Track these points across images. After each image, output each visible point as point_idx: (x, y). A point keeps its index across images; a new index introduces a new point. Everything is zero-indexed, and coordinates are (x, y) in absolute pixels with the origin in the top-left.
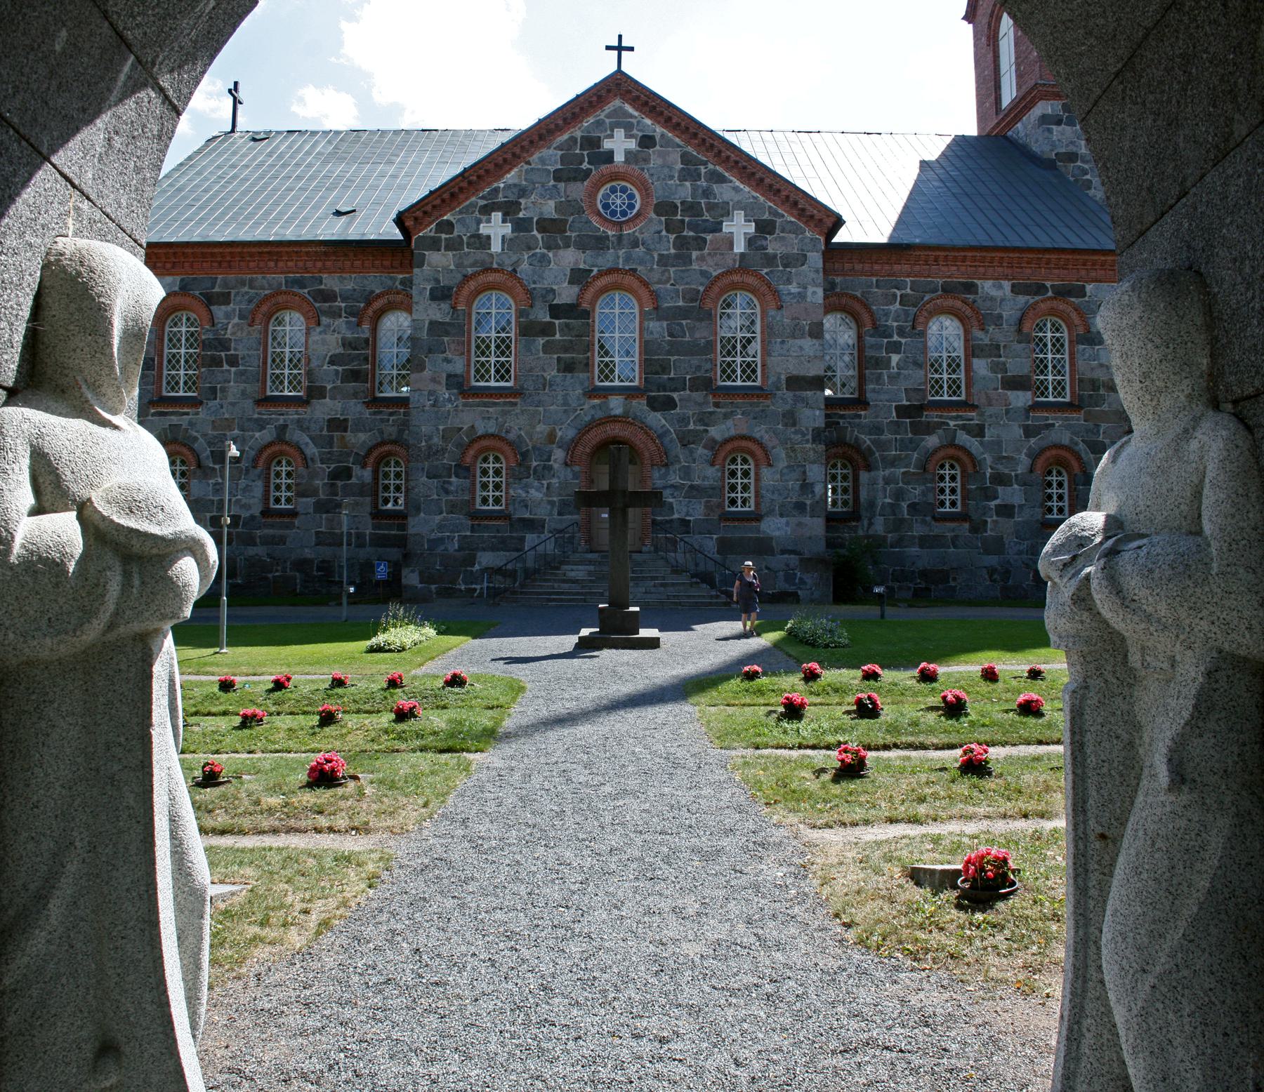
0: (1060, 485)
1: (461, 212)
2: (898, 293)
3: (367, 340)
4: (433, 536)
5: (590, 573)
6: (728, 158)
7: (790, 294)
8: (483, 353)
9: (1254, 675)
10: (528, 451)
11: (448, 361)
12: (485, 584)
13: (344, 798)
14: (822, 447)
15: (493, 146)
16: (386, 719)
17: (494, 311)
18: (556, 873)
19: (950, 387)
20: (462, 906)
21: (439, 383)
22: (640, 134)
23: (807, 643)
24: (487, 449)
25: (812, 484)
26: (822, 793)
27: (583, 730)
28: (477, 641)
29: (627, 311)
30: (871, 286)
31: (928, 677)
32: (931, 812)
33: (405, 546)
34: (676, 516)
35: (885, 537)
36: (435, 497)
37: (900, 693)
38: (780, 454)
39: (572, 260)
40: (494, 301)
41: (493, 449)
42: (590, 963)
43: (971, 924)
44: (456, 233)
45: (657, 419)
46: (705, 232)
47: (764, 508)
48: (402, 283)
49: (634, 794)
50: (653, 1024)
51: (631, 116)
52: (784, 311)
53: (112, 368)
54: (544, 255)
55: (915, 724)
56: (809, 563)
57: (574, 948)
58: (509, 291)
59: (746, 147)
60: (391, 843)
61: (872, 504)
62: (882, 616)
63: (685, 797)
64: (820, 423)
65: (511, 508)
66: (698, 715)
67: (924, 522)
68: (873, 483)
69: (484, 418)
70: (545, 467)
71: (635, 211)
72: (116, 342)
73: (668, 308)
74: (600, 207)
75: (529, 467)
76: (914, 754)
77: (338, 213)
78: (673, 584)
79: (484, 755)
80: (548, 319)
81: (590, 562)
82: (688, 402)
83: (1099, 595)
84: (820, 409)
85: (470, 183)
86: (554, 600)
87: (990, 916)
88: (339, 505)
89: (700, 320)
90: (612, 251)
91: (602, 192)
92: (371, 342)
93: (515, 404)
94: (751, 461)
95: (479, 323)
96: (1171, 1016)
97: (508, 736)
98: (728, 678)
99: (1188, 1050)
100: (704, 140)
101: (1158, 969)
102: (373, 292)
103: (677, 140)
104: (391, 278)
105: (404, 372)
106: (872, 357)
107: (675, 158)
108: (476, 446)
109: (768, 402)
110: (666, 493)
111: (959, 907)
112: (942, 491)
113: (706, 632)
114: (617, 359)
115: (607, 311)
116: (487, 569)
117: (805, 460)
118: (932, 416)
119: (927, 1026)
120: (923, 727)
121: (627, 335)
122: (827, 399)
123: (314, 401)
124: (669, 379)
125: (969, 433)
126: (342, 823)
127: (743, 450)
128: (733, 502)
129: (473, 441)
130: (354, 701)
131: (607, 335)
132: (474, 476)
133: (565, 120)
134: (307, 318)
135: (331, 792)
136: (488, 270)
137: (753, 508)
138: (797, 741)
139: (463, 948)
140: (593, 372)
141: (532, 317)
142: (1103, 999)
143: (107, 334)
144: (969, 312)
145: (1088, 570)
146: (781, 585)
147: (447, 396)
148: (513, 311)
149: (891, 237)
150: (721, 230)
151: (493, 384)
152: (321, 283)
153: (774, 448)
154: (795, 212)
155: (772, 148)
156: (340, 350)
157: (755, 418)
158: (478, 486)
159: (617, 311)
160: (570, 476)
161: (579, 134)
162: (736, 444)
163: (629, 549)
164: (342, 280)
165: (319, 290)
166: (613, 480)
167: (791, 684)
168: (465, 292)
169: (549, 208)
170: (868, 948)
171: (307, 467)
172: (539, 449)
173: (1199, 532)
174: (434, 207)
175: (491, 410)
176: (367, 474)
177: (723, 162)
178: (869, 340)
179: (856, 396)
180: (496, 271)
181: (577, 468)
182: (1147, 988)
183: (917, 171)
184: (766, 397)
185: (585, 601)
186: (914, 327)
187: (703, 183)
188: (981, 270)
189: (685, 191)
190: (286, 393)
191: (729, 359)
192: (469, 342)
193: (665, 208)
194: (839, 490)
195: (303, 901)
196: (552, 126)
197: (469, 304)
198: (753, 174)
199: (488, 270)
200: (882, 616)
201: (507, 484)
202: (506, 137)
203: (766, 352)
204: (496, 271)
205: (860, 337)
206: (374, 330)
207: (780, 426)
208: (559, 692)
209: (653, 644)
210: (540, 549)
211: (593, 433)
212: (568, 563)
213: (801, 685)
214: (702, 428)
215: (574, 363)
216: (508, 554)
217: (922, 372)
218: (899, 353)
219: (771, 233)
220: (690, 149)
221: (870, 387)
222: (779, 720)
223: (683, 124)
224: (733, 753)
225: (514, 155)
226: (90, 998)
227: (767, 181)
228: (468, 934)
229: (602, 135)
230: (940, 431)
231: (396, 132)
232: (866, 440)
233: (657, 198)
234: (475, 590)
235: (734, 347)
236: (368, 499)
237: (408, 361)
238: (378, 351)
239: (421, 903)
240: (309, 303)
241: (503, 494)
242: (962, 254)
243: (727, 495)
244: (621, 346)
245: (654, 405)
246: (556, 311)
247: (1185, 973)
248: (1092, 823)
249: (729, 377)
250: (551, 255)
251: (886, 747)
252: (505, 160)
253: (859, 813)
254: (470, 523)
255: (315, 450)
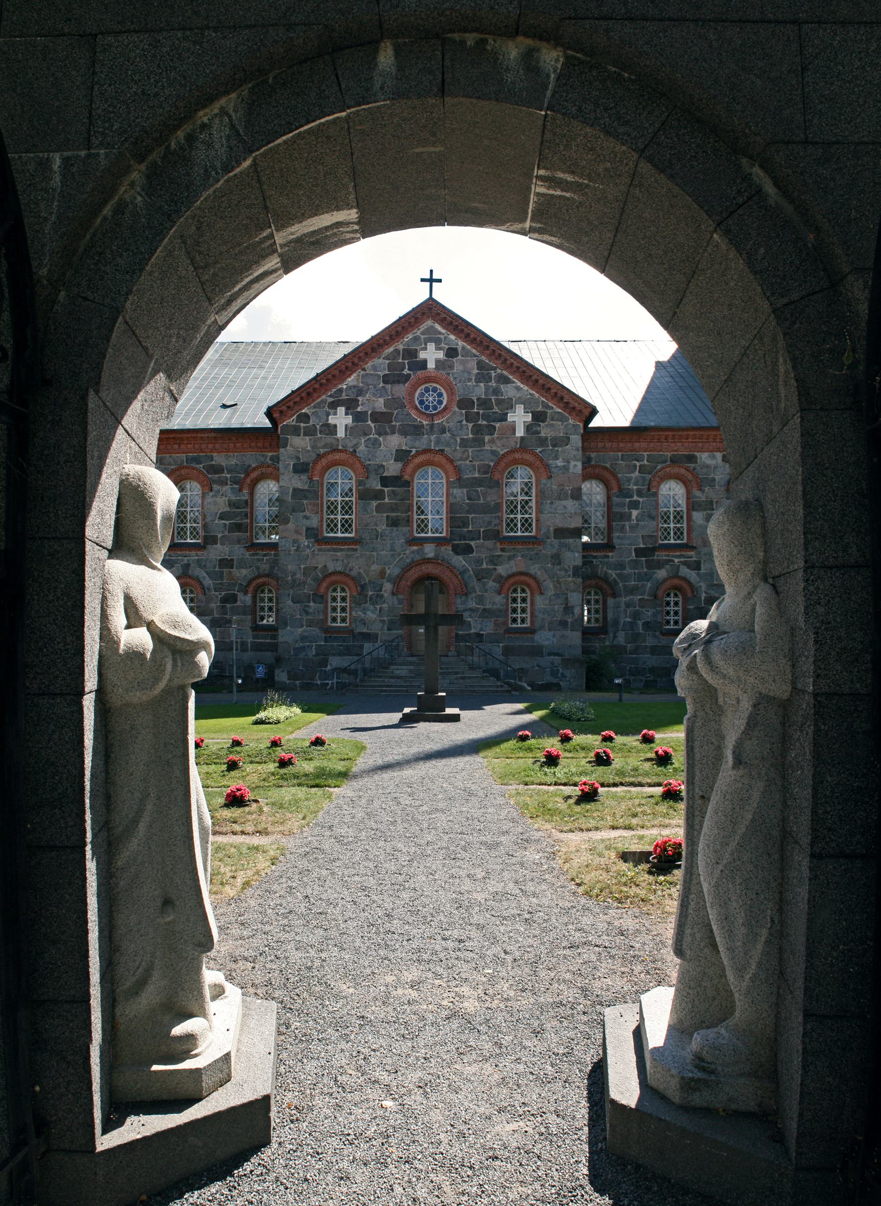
0: (676, 604)
1: (315, 407)
2: (638, 464)
3: (246, 502)
4: (297, 645)
5: (410, 671)
6: (512, 364)
7: (557, 467)
8: (332, 512)
9: (779, 707)
10: (365, 584)
11: (306, 518)
12: (335, 680)
13: (249, 813)
14: (579, 580)
15: (339, 356)
16: (272, 767)
17: (340, 481)
18: (393, 855)
19: (675, 533)
20: (333, 874)
21: (301, 534)
22: (447, 347)
23: (565, 718)
24: (336, 582)
25: (572, 607)
26: (568, 811)
27: (408, 772)
28: (330, 717)
29: (437, 481)
30: (617, 460)
31: (648, 740)
32: (640, 823)
33: (277, 650)
34: (473, 631)
35: (625, 647)
36: (299, 616)
37: (627, 751)
38: (549, 586)
39: (397, 443)
40: (340, 474)
41: (345, 583)
42: (415, 903)
43: (656, 882)
44: (311, 423)
45: (459, 561)
46: (494, 421)
47: (537, 625)
48: (272, 459)
49: (443, 811)
50: (456, 933)
51: (440, 333)
52: (553, 480)
53: (157, 537)
54: (376, 440)
55: (635, 769)
56: (568, 662)
57: (405, 895)
58: (351, 466)
59: (526, 355)
60: (284, 840)
61: (616, 622)
62: (620, 700)
63: (477, 813)
64: (579, 562)
65: (353, 625)
66: (486, 764)
67: (654, 636)
68: (617, 606)
69: (333, 560)
70: (378, 596)
71: (443, 406)
72: (159, 523)
73: (467, 478)
74: (417, 403)
75: (366, 596)
76: (633, 789)
77: (224, 406)
78: (469, 678)
79: (340, 789)
80: (379, 487)
81: (411, 663)
82: (481, 548)
83: (700, 665)
84: (578, 552)
85: (321, 385)
86: (385, 691)
87: (669, 878)
88: (230, 622)
89: (491, 487)
90: (426, 436)
91: (418, 391)
92: (250, 503)
93: (356, 550)
94: (528, 591)
95: (328, 490)
96: (730, 886)
97: (355, 776)
98: (508, 740)
99: (738, 903)
100: (494, 351)
101: (725, 862)
102: (250, 466)
103: (474, 351)
104: (263, 456)
105: (273, 524)
106: (617, 513)
107: (472, 365)
108: (328, 580)
109: (540, 548)
110: (466, 614)
111: (650, 873)
112: (668, 613)
113: (493, 711)
114: (430, 517)
115: (422, 481)
116: (336, 669)
117: (567, 589)
118: (661, 555)
119: (623, 935)
120: (641, 771)
121: (437, 499)
122: (585, 545)
123: (209, 546)
124: (468, 531)
125: (689, 567)
126: (249, 828)
127: (522, 583)
128: (514, 620)
129: (325, 577)
130: (248, 756)
131: (422, 499)
132: (327, 602)
133: (391, 336)
134: (203, 486)
135: (241, 810)
136: (335, 450)
137: (529, 625)
138: (553, 780)
139: (335, 896)
140: (413, 526)
141: (368, 486)
142: (699, 883)
143: (154, 519)
144: (690, 477)
145: (696, 651)
146: (549, 679)
147: (306, 544)
148: (354, 482)
149: (633, 422)
150: (506, 420)
151: (339, 535)
152: (212, 460)
153: (544, 581)
154: (561, 405)
155: (545, 354)
156: (227, 509)
157: (531, 559)
158: (329, 609)
159: (430, 481)
160: (396, 602)
161: (401, 347)
162: (517, 578)
163: (439, 653)
164: (227, 457)
165: (211, 465)
166: (428, 605)
167: (552, 744)
168: (319, 467)
169: (380, 404)
170: (591, 896)
171: (205, 594)
172: (373, 583)
173: (753, 631)
174: (295, 403)
175: (338, 554)
176: (248, 599)
177: (508, 368)
178: (615, 500)
179: (605, 541)
180: (341, 451)
181: (401, 597)
182: (719, 872)
183: (654, 369)
184: (539, 545)
185: (407, 691)
186: (649, 490)
187: (493, 384)
188: (700, 445)
189: (480, 391)
190: (189, 541)
191: (512, 516)
192: (322, 503)
193: (465, 403)
194: (593, 611)
195: (231, 871)
196: (381, 341)
197: (322, 476)
198: (531, 376)
199: (335, 450)
200: (620, 700)
201: (351, 608)
202: (347, 349)
203: (539, 511)
204: (341, 451)
205: (609, 498)
206: (252, 494)
207: (549, 565)
208: (390, 749)
209: (455, 718)
210: (375, 654)
211: (412, 571)
212: (395, 664)
213: (558, 745)
214: (492, 567)
215: (398, 520)
216: (351, 657)
217: (655, 523)
218: (638, 509)
219: (543, 421)
220: (483, 358)
221: (616, 534)
222: (542, 766)
223: (478, 339)
224: (510, 787)
225: (353, 363)
226: (159, 875)
227: (541, 381)
228: (338, 888)
229: (418, 348)
230: (668, 567)
231: (265, 344)
232: (613, 574)
233: (459, 396)
234: (328, 684)
235: (516, 507)
236: (249, 617)
237: (276, 516)
238: (255, 509)
239: (306, 873)
240: (204, 475)
241: (348, 615)
242: (685, 433)
243: (510, 616)
244: (433, 507)
245: (457, 550)
246: (385, 481)
247: (738, 863)
248: (697, 790)
249: (512, 530)
250: (381, 439)
251: (615, 785)
252: (347, 368)
253: (592, 823)
254: (324, 635)
255: (211, 582)
